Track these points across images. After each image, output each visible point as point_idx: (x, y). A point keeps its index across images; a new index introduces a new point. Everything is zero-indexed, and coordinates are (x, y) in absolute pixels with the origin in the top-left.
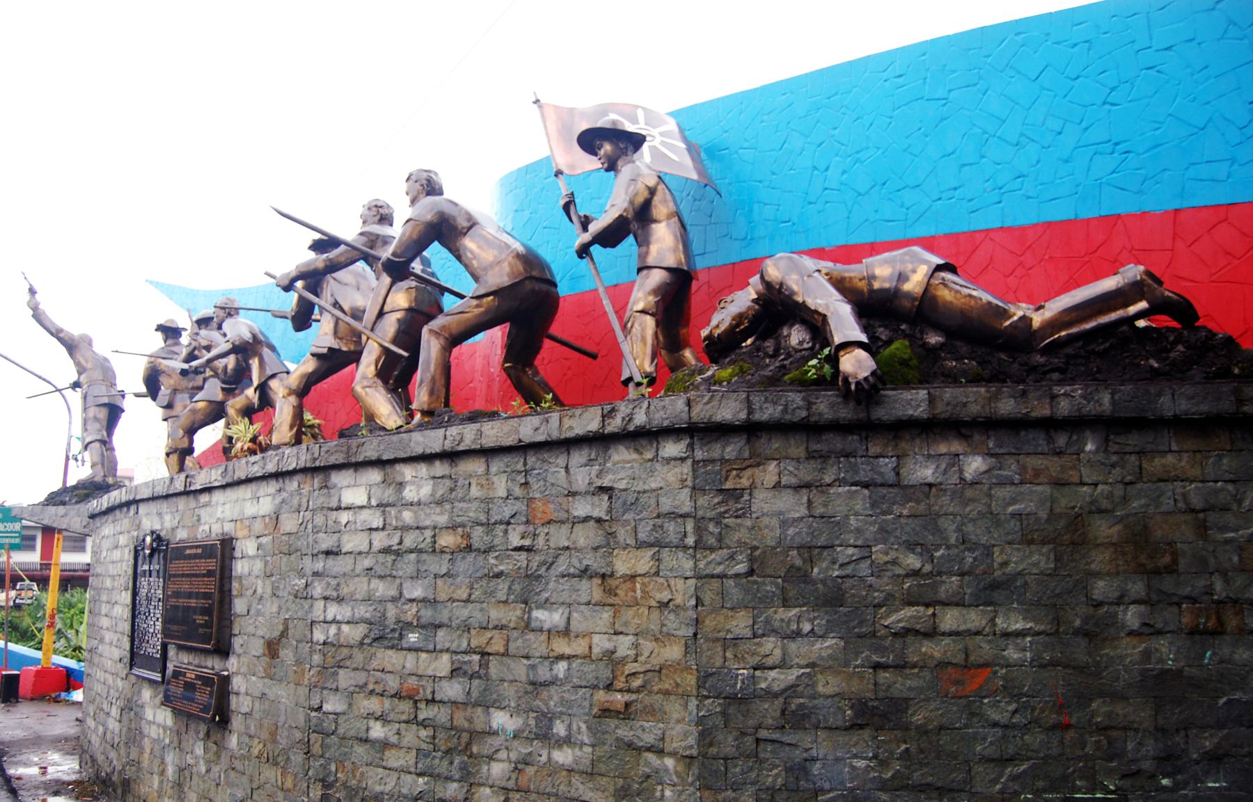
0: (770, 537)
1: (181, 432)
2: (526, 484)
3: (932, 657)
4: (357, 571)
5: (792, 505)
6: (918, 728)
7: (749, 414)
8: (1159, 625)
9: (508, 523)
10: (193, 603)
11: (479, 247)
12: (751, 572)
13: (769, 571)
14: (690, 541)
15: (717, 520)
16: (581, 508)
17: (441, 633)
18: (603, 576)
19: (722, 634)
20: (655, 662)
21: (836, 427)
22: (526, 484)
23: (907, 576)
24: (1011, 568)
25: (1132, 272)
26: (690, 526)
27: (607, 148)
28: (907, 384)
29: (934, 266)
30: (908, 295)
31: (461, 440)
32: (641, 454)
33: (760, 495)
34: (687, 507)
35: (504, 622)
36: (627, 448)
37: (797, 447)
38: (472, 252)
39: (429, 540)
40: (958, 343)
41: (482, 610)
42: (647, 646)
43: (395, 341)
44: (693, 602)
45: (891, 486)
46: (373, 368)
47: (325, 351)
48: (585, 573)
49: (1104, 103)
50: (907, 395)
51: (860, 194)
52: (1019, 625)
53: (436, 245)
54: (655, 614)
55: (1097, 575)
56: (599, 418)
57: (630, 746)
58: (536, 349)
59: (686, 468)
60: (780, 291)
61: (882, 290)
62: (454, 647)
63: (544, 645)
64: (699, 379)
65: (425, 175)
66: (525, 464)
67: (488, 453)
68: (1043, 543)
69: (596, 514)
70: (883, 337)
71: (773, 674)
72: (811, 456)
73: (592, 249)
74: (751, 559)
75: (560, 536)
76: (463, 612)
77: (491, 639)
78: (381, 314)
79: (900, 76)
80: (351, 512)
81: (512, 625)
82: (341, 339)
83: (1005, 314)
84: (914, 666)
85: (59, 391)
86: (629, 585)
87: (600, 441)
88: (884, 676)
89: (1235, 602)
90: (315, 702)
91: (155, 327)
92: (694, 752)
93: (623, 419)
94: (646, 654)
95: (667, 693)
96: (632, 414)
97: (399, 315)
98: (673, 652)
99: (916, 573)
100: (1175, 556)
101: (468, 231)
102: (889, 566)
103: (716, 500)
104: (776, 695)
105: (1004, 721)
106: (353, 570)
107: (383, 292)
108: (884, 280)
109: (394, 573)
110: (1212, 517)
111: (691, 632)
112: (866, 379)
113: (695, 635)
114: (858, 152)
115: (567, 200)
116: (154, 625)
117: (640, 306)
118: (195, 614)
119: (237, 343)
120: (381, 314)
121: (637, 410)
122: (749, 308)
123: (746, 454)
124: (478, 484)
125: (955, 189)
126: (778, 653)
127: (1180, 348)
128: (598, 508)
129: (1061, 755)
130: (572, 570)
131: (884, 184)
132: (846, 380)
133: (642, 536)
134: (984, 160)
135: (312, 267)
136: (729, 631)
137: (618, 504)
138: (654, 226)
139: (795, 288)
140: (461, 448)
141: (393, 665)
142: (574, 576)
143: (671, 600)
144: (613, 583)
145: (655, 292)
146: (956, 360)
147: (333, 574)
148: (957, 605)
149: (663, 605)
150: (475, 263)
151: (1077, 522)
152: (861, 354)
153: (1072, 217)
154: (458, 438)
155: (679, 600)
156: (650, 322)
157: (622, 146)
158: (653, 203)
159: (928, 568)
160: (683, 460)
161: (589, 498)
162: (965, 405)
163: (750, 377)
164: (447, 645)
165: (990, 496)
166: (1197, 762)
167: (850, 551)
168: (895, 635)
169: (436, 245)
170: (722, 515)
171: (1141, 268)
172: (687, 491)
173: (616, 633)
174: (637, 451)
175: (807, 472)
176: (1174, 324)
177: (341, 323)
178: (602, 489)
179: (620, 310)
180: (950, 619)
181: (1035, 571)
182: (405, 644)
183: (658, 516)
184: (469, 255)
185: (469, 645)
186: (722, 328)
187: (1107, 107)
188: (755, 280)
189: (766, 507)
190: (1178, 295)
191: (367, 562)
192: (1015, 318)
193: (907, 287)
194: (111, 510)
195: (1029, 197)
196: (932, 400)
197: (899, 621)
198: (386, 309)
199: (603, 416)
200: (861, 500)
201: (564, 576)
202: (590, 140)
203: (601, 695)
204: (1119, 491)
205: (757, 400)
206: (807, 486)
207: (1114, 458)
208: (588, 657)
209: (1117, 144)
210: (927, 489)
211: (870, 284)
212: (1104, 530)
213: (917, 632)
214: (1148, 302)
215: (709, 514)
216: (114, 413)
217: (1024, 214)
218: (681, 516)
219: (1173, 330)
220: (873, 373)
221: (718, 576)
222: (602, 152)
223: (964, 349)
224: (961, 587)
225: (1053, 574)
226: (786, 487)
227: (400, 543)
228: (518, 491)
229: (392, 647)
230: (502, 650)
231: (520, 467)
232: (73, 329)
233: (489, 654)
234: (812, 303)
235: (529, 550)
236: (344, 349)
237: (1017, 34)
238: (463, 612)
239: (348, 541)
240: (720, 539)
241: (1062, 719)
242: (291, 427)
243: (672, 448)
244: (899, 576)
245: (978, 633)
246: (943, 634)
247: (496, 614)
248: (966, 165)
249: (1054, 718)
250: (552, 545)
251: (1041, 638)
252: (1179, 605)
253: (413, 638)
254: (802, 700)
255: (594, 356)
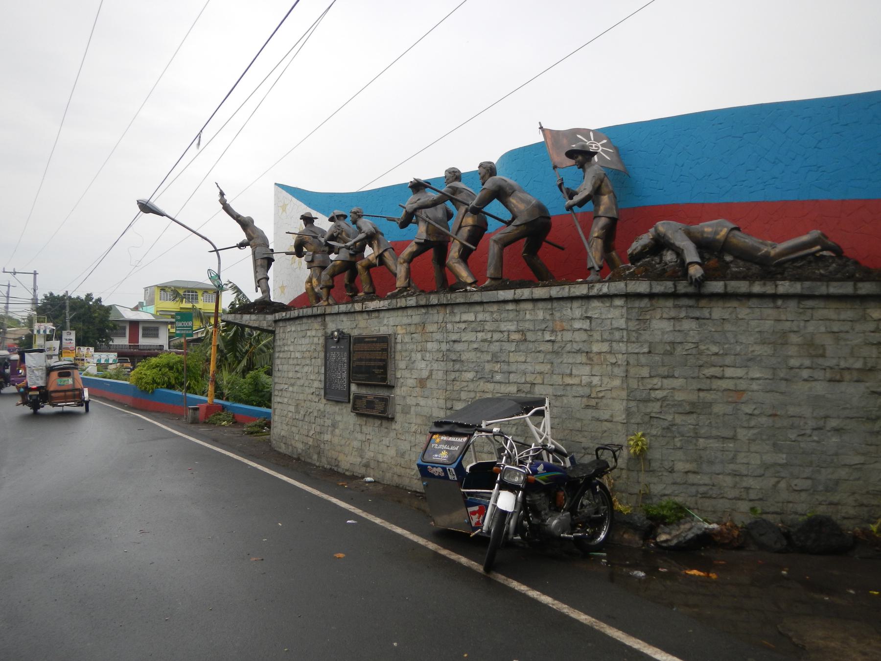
0: (658, 338)
1: (328, 277)
2: (552, 314)
3: (722, 387)
4: (470, 349)
5: (667, 326)
6: (715, 414)
7: (651, 289)
8: (816, 377)
9: (544, 330)
10: (372, 364)
11: (517, 202)
12: (650, 352)
13: (657, 352)
14: (625, 340)
15: (637, 331)
16: (577, 325)
17: (512, 375)
18: (587, 352)
19: (637, 376)
20: (609, 386)
21: (686, 295)
22: (552, 314)
23: (713, 355)
24: (756, 353)
25: (815, 233)
26: (625, 333)
27: (580, 158)
28: (715, 279)
29: (730, 229)
30: (718, 241)
31: (523, 295)
32: (604, 304)
33: (654, 322)
34: (624, 326)
35: (542, 370)
36: (599, 302)
37: (670, 303)
38: (513, 204)
39: (506, 336)
40: (739, 261)
41: (531, 366)
42: (606, 380)
43: (468, 240)
44: (626, 363)
45: (707, 319)
46: (457, 254)
47: (423, 241)
48: (579, 351)
49: (815, 147)
50: (714, 283)
51: (697, 179)
52: (758, 375)
53: (496, 201)
54: (609, 368)
55: (791, 357)
56: (587, 289)
57: (598, 420)
58: (538, 246)
59: (624, 310)
60: (663, 237)
61: (707, 238)
62: (518, 381)
63: (561, 380)
64: (627, 272)
65: (489, 165)
66: (552, 306)
67: (534, 301)
68: (769, 344)
69: (585, 327)
70: (707, 257)
71: (657, 392)
72: (675, 306)
73: (573, 208)
74: (650, 347)
75: (568, 336)
76: (523, 367)
77: (536, 378)
78: (460, 227)
79: (720, 124)
80: (466, 323)
81: (545, 372)
82: (429, 235)
83: (759, 250)
84: (714, 390)
85: (216, 250)
86: (598, 356)
87: (587, 298)
88: (702, 394)
89: (848, 369)
90: (449, 406)
91: (300, 217)
92: (625, 421)
93: (598, 290)
94: (605, 383)
95: (614, 399)
96: (601, 288)
97: (469, 228)
98: (617, 382)
99: (716, 354)
100: (824, 349)
101: (512, 193)
102: (705, 351)
103: (636, 323)
104: (658, 400)
105: (750, 412)
106: (468, 349)
107: (461, 216)
108: (708, 233)
109: (489, 350)
110: (842, 335)
111: (624, 375)
112: (699, 277)
113: (627, 376)
114: (699, 159)
115: (560, 182)
116: (343, 375)
117: (596, 235)
118: (374, 369)
119: (369, 234)
120: (460, 227)
121: (603, 286)
122: (649, 242)
123: (649, 306)
124: (529, 313)
125: (744, 181)
126: (660, 384)
127: (834, 265)
128: (586, 325)
129: (773, 426)
130: (573, 350)
131: (710, 175)
132: (691, 277)
133: (605, 337)
134: (758, 169)
135: (426, 204)
136: (640, 375)
137: (594, 324)
138: (602, 197)
139: (670, 236)
140: (522, 298)
141: (489, 389)
142: (574, 353)
143: (616, 362)
144: (592, 355)
145: (603, 228)
146: (737, 268)
147: (458, 350)
148: (733, 367)
149: (612, 364)
150: (515, 209)
151: (784, 334)
152: (697, 267)
153: (796, 199)
154: (521, 294)
155: (620, 362)
156: (600, 241)
157: (587, 157)
158: (602, 186)
159: (721, 352)
160: (622, 307)
161: (581, 321)
162: (739, 288)
163: (649, 273)
164: (515, 380)
165: (748, 324)
166: (829, 431)
167: (690, 344)
168: (707, 378)
169: (496, 201)
170: (638, 329)
171: (819, 231)
172: (624, 320)
173: (592, 375)
174: (602, 302)
175: (673, 313)
176: (832, 254)
177: (430, 226)
178: (587, 318)
179: (587, 236)
180: (729, 372)
181: (765, 354)
182: (495, 379)
183: (612, 329)
184: (513, 205)
185: (525, 380)
186: (637, 251)
187: (816, 149)
188: (652, 230)
189: (656, 327)
190: (834, 243)
191: (475, 346)
192: (763, 251)
193: (718, 237)
194: (299, 318)
195: (777, 188)
196: (726, 286)
197: (709, 372)
198: (463, 224)
199: (589, 288)
200: (693, 324)
201: (569, 352)
202: (571, 154)
203: (585, 400)
204: (802, 324)
205: (654, 283)
206: (673, 318)
207: (801, 310)
208: (580, 385)
209: (820, 167)
210: (722, 321)
211: (702, 235)
212: (794, 338)
213: (716, 377)
214: (821, 245)
215: (634, 329)
216: (269, 261)
217: (774, 195)
218: (621, 329)
219: (831, 257)
220: (702, 275)
221: (636, 353)
222: (578, 159)
223: (741, 263)
224: (735, 360)
225: (773, 355)
226: (664, 318)
227: (492, 338)
228: (548, 317)
229: (488, 382)
230: (541, 382)
231: (549, 307)
232: (244, 213)
233: (535, 384)
234: (677, 243)
235: (553, 342)
236: (432, 240)
237: (778, 109)
238: (523, 367)
239: (465, 336)
240: (637, 338)
241: (774, 412)
242: (406, 279)
243: (618, 302)
244: (709, 355)
245: (741, 378)
246: (727, 378)
247: (539, 368)
248: (750, 170)
249: (770, 412)
250: (564, 340)
251: (767, 381)
252: (825, 369)
253: (498, 377)
254: (668, 402)
255: (563, 249)
